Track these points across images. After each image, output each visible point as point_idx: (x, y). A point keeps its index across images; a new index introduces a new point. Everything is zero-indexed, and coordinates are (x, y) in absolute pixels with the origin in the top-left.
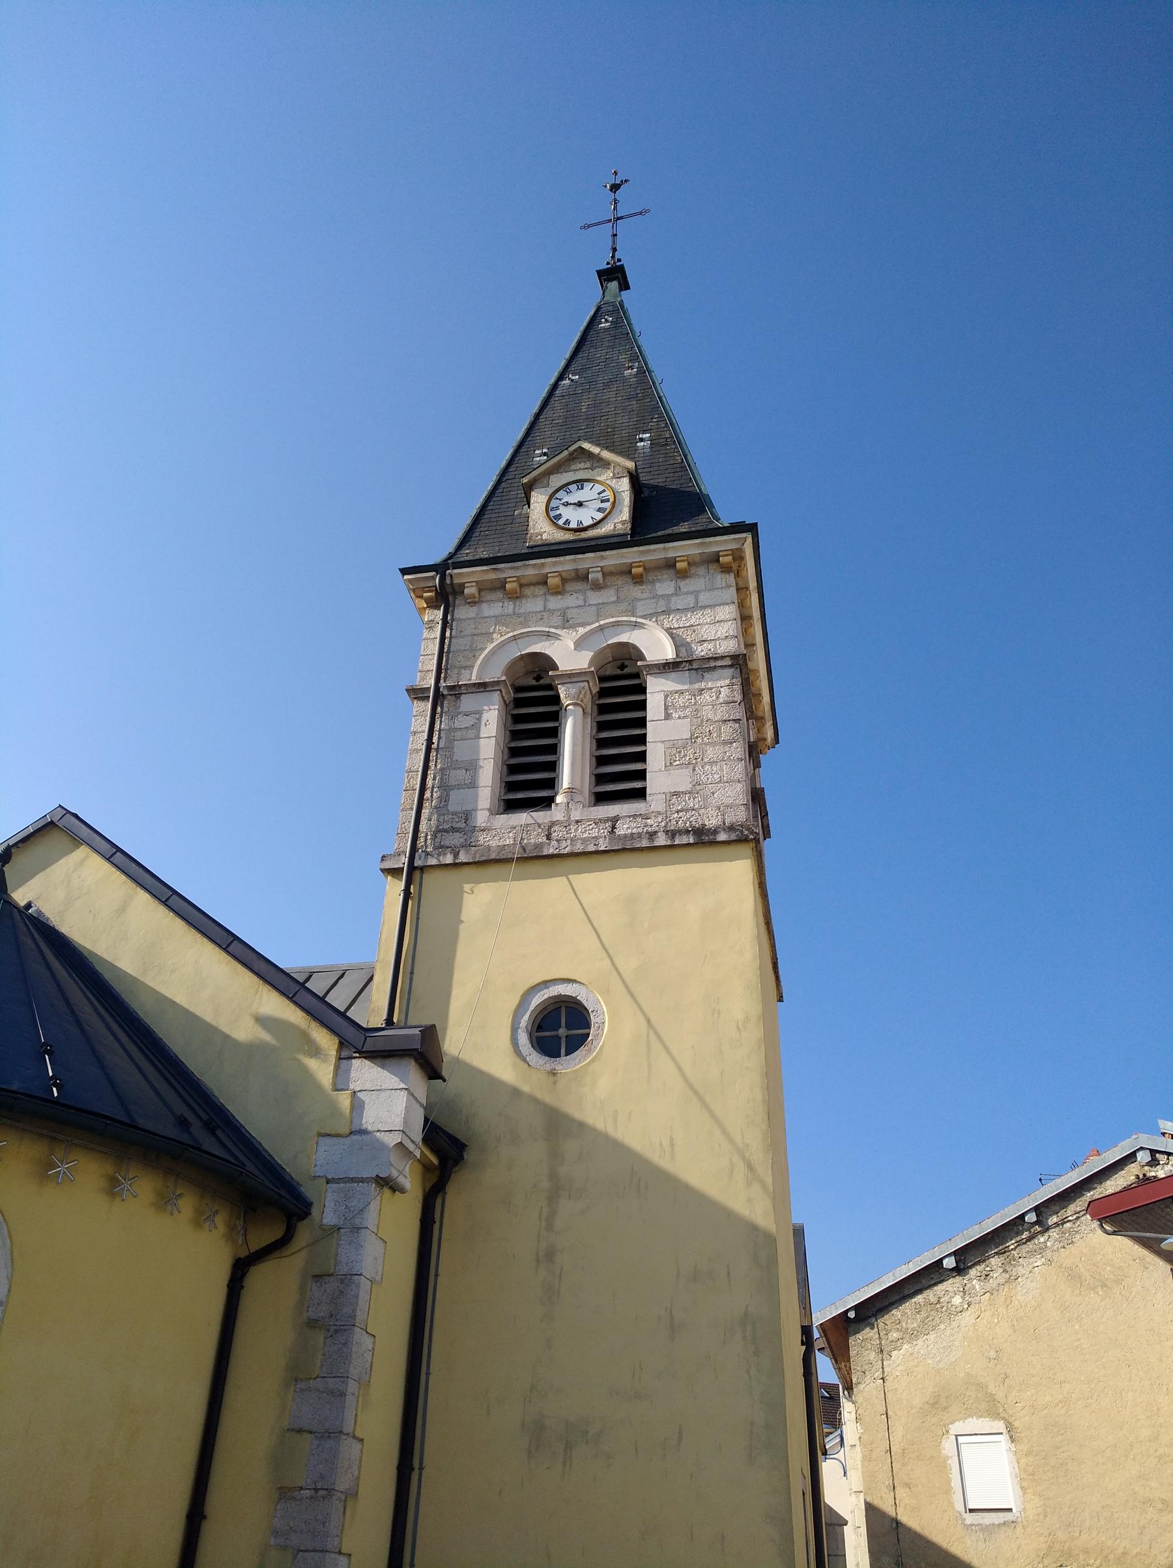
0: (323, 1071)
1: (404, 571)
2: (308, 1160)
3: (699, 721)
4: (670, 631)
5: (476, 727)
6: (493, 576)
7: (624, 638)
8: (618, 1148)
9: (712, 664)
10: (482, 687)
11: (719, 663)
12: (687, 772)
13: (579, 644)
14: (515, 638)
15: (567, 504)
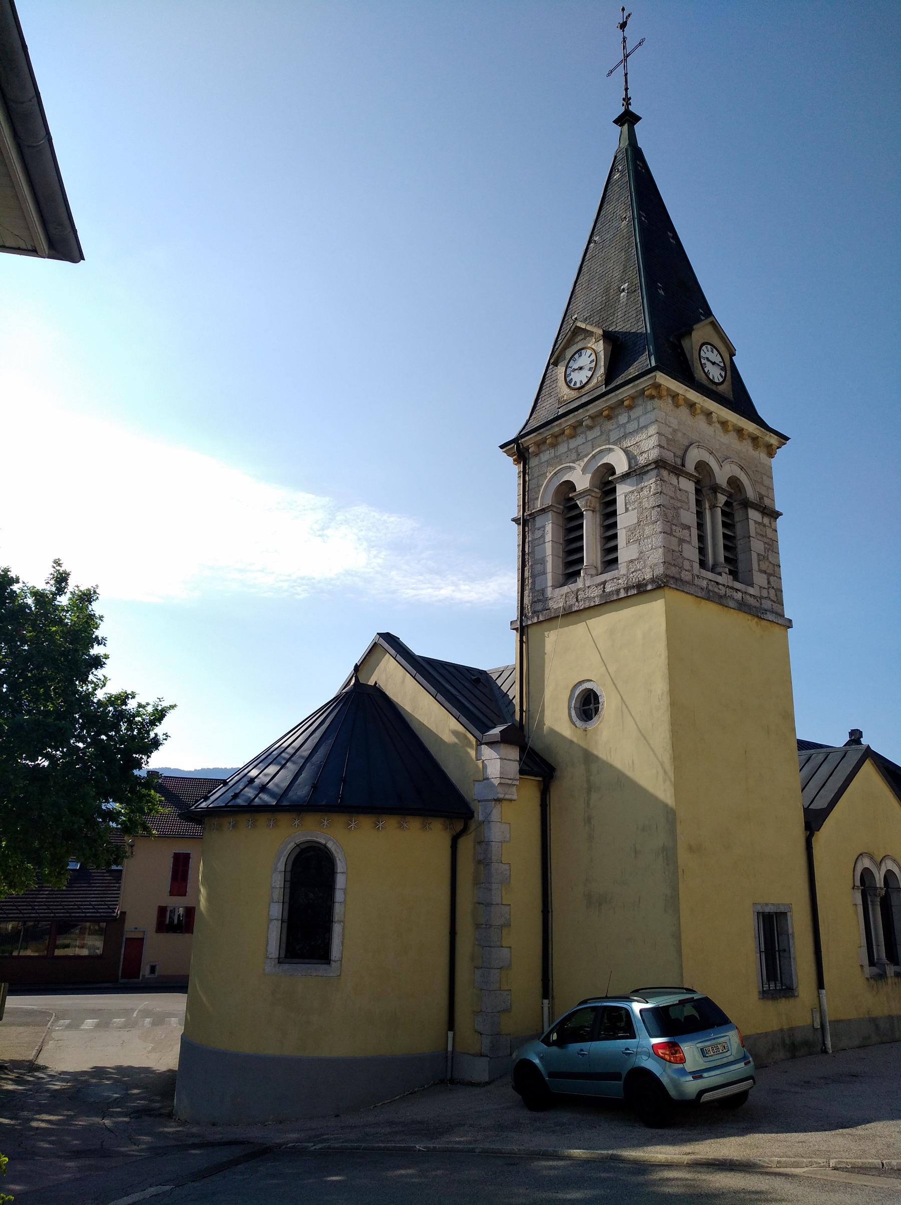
0: (473, 753)
1: (502, 447)
2: (472, 792)
3: (641, 510)
4: (626, 451)
5: (543, 536)
6: (540, 437)
7: (605, 461)
8: (611, 767)
9: (646, 469)
10: (543, 511)
11: (649, 468)
12: (636, 546)
13: (584, 471)
14: (556, 474)
15: (574, 370)
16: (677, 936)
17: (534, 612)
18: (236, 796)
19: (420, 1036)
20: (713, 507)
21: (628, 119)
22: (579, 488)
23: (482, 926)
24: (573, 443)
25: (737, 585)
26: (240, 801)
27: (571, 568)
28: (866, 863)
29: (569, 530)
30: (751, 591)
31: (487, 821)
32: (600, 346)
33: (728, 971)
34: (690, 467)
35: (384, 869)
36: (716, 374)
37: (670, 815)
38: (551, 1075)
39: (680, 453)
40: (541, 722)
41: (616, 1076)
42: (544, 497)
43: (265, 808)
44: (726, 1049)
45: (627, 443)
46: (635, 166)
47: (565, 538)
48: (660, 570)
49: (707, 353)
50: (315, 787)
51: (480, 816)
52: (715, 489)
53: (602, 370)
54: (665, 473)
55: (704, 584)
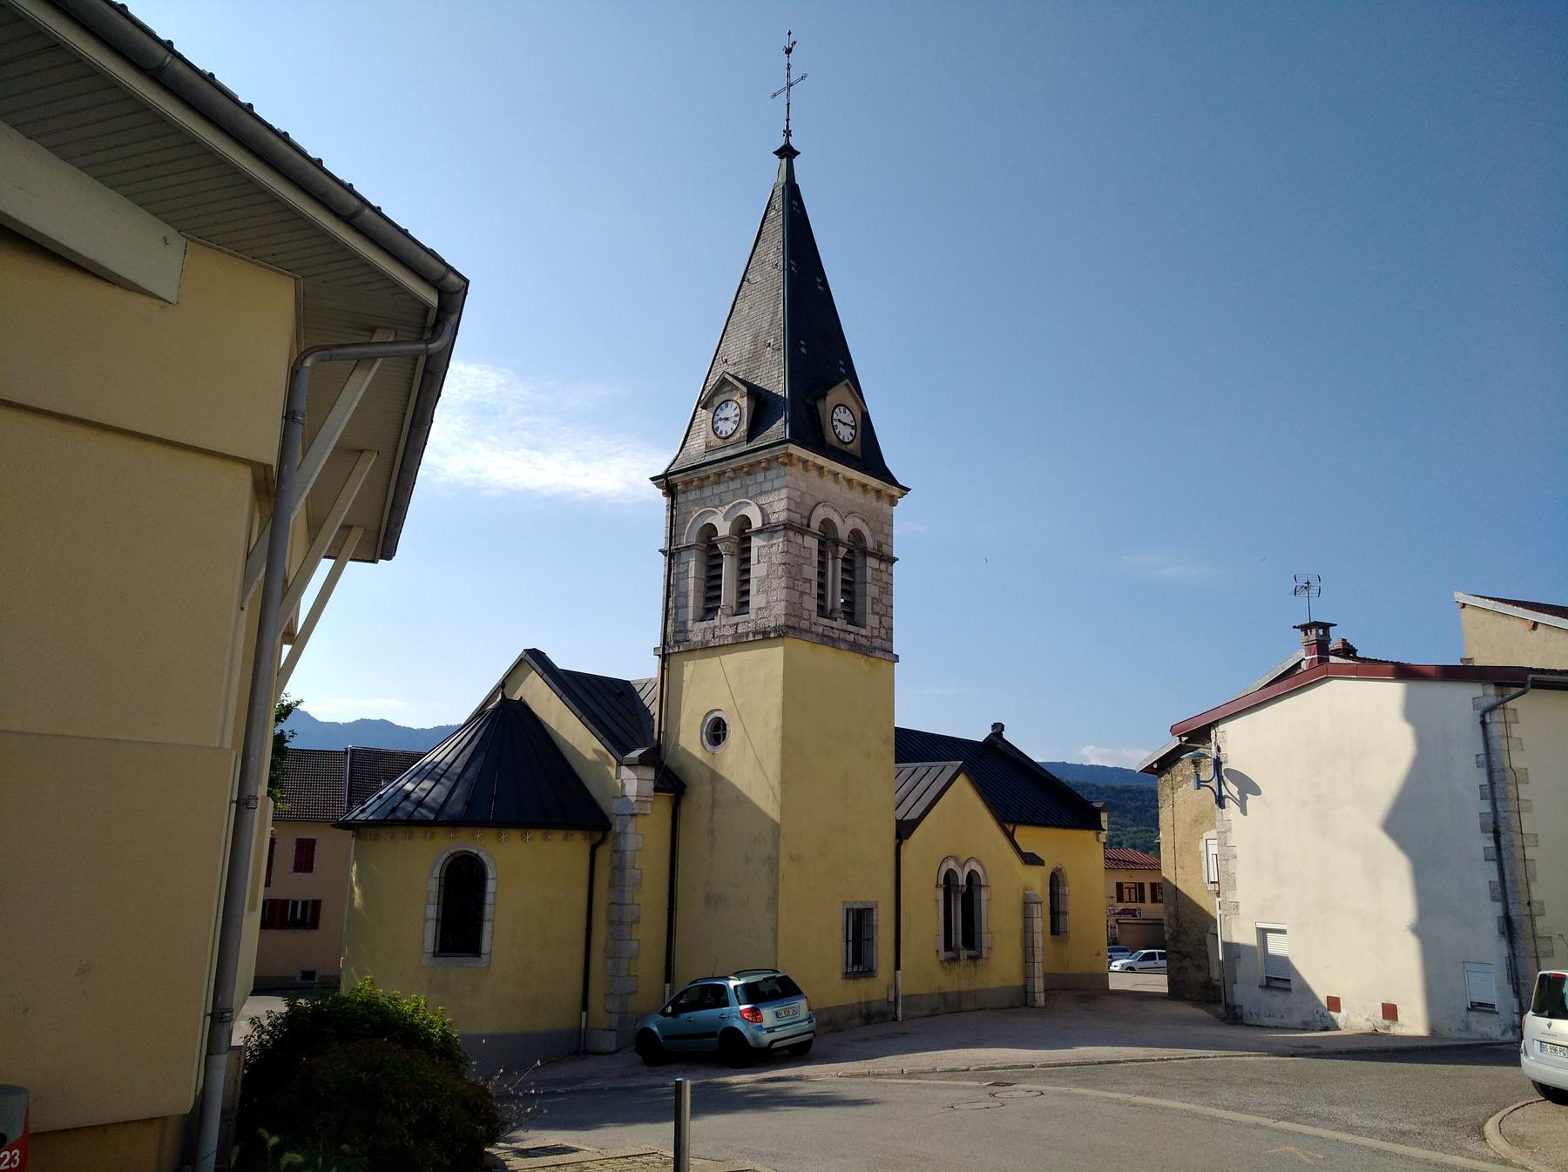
0: (613, 771)
2: (611, 807)
7: (743, 512)
8: (733, 786)
13: (725, 518)
16: (775, 930)
17: (676, 642)
18: (394, 810)
19: (558, 1015)
20: (835, 558)
21: (787, 153)
22: (720, 534)
23: (615, 923)
24: (717, 489)
25: (851, 628)
26: (399, 814)
27: (709, 608)
28: (951, 865)
29: (710, 578)
30: (863, 632)
31: (623, 833)
32: (744, 402)
33: (815, 956)
34: (815, 525)
35: (530, 875)
36: (846, 433)
37: (776, 829)
38: (666, 1038)
39: (806, 514)
40: (677, 743)
41: (713, 1034)
42: (689, 536)
43: (424, 823)
44: (796, 1012)
45: (763, 500)
46: (791, 206)
47: (704, 574)
48: (782, 621)
49: (842, 415)
50: (468, 804)
51: (617, 828)
52: (837, 542)
53: (744, 427)
54: (791, 534)
55: (820, 629)
